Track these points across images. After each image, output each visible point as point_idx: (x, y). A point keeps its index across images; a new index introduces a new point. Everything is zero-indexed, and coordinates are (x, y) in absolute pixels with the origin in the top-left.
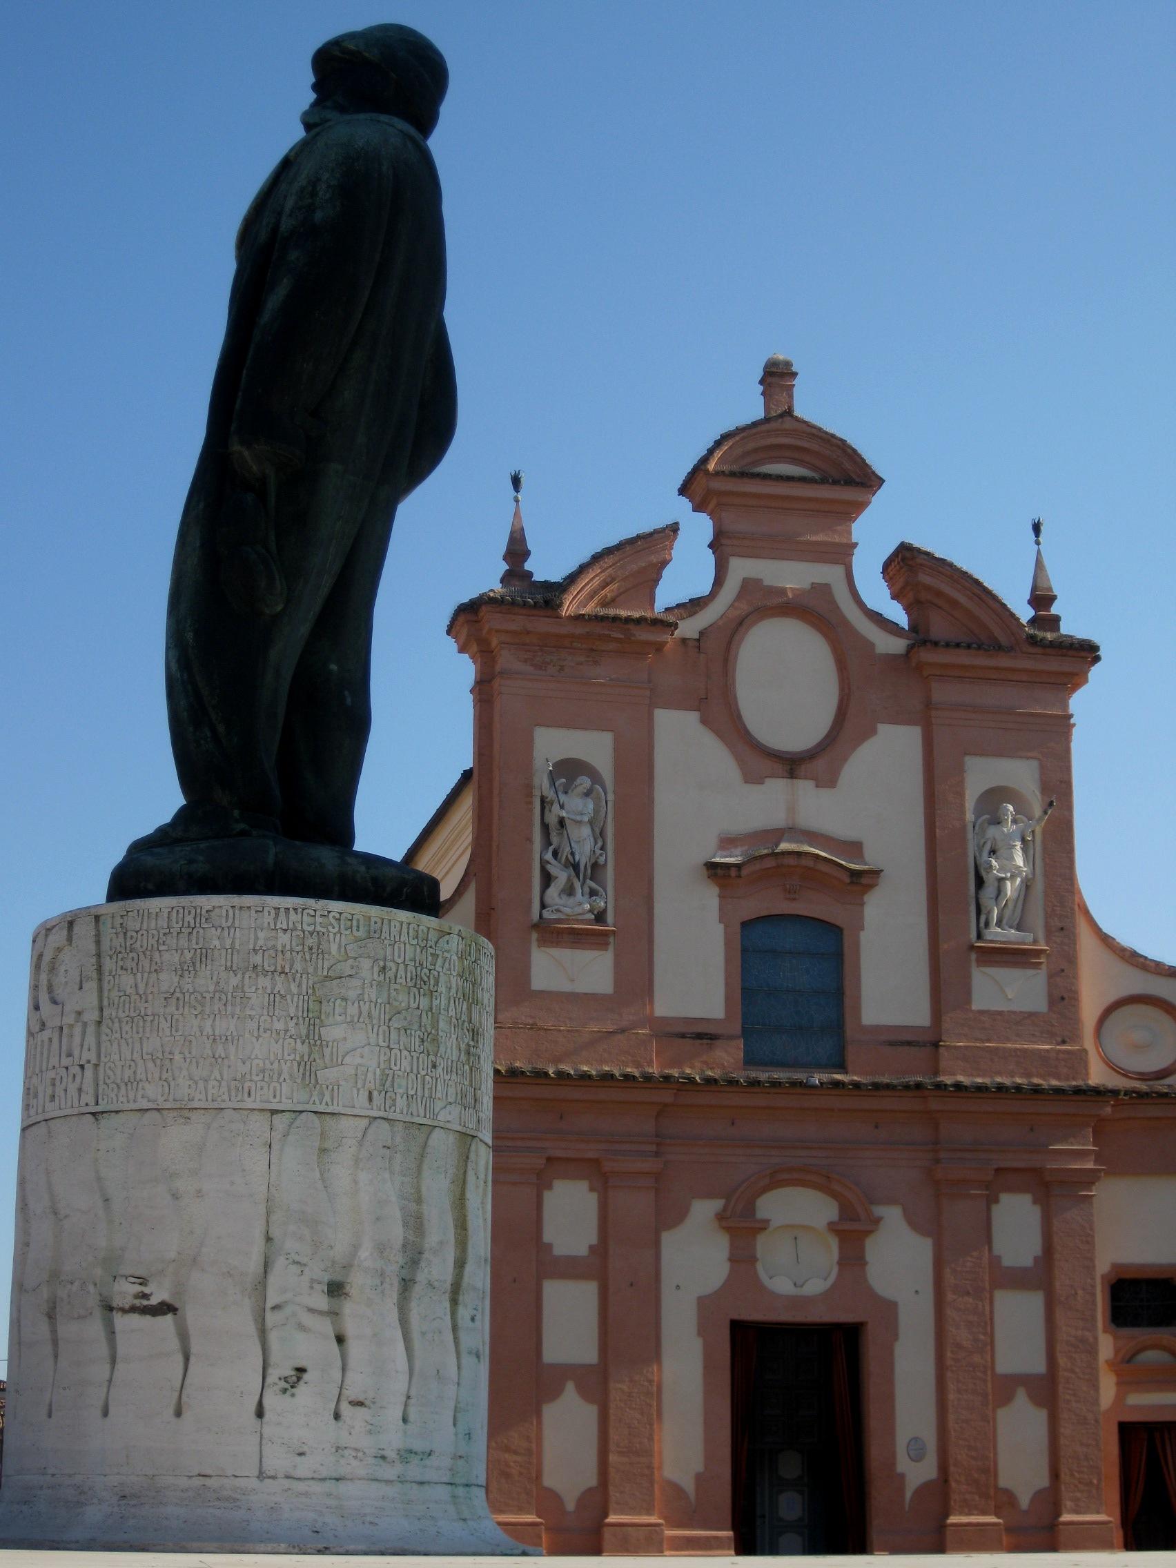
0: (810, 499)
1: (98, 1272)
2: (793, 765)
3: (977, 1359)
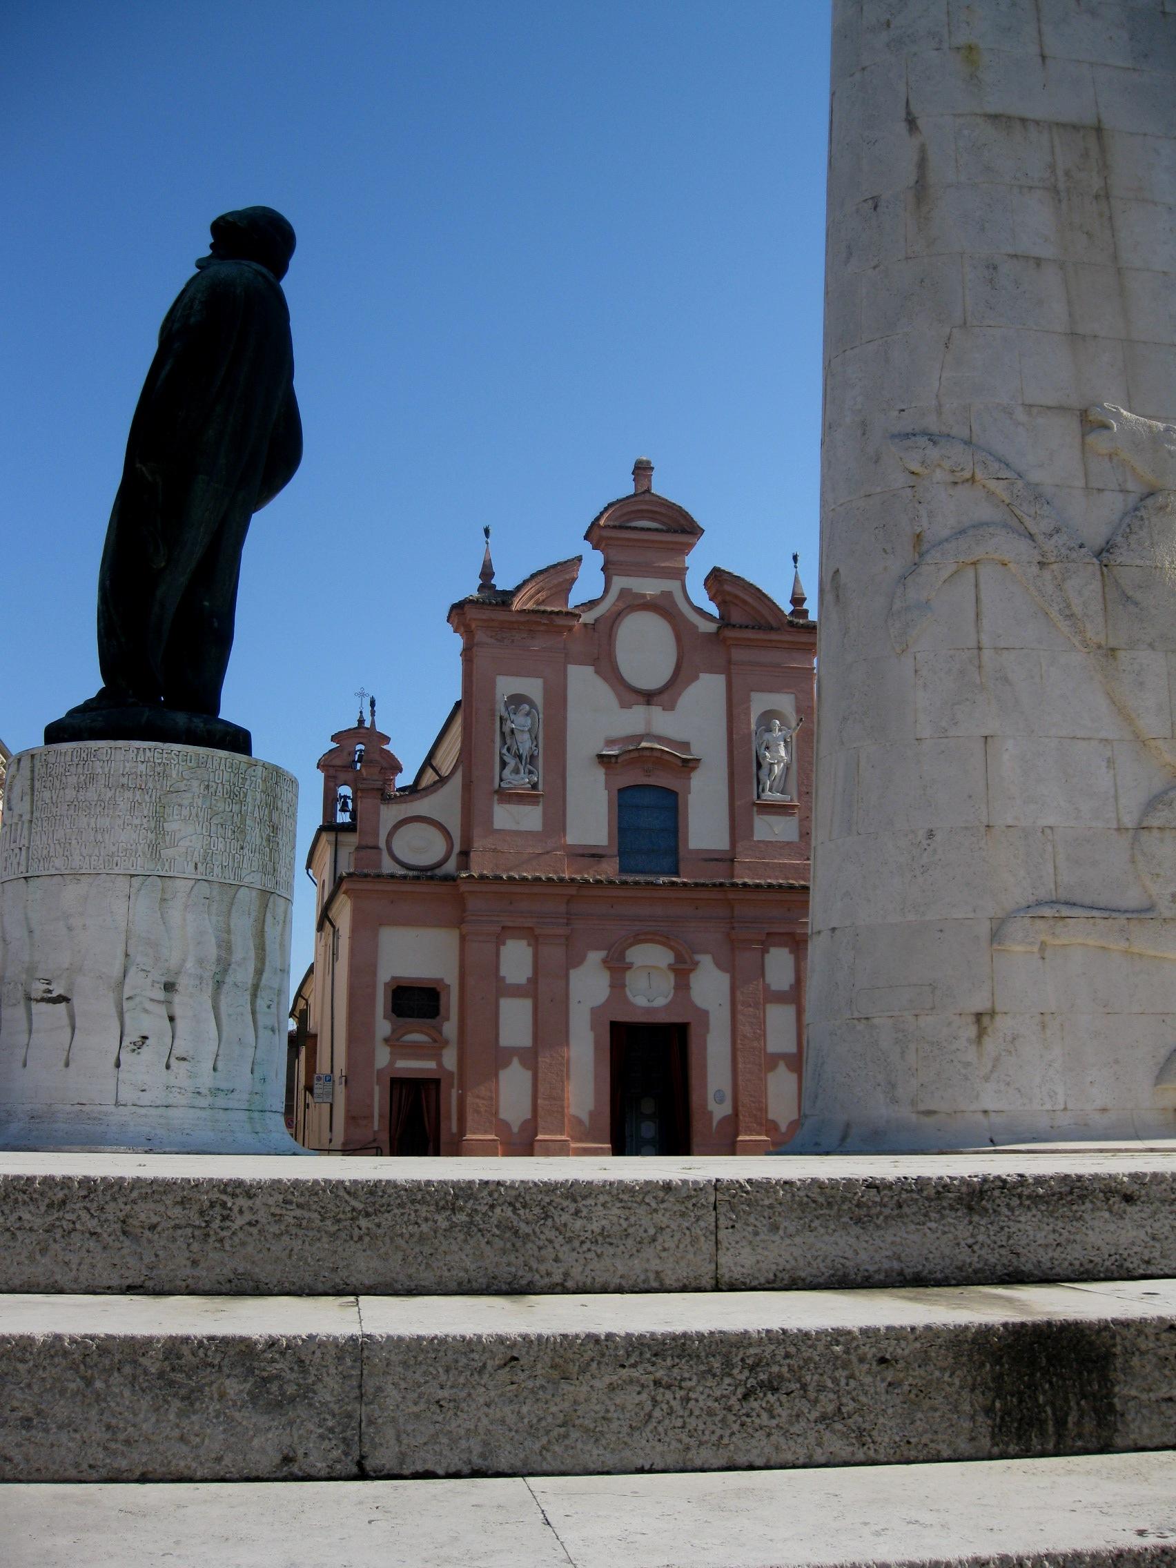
0: (661, 542)
1: (24, 976)
2: (649, 697)
3: (755, 1044)
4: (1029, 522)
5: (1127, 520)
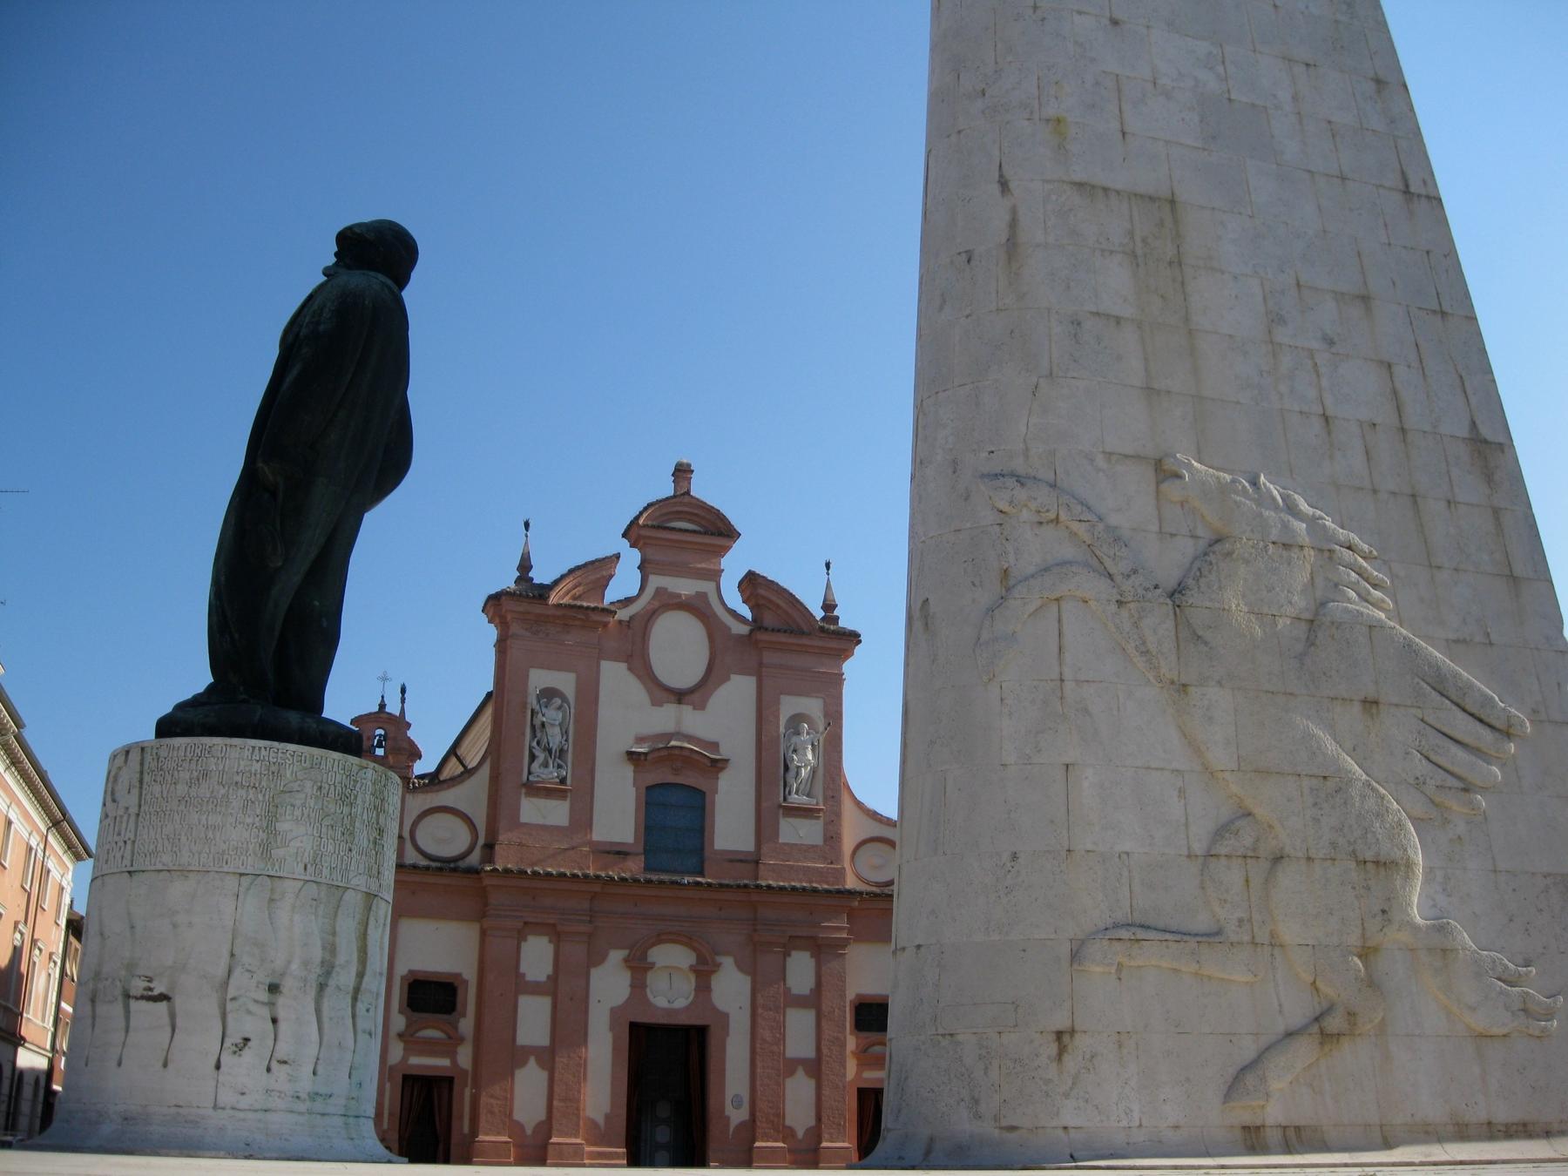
1: (123, 973)
2: (680, 696)
3: (775, 1048)
4: (1108, 562)
5: (1197, 564)
